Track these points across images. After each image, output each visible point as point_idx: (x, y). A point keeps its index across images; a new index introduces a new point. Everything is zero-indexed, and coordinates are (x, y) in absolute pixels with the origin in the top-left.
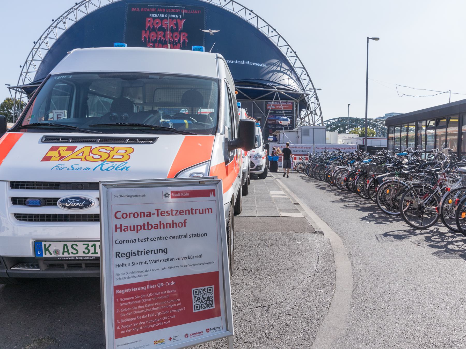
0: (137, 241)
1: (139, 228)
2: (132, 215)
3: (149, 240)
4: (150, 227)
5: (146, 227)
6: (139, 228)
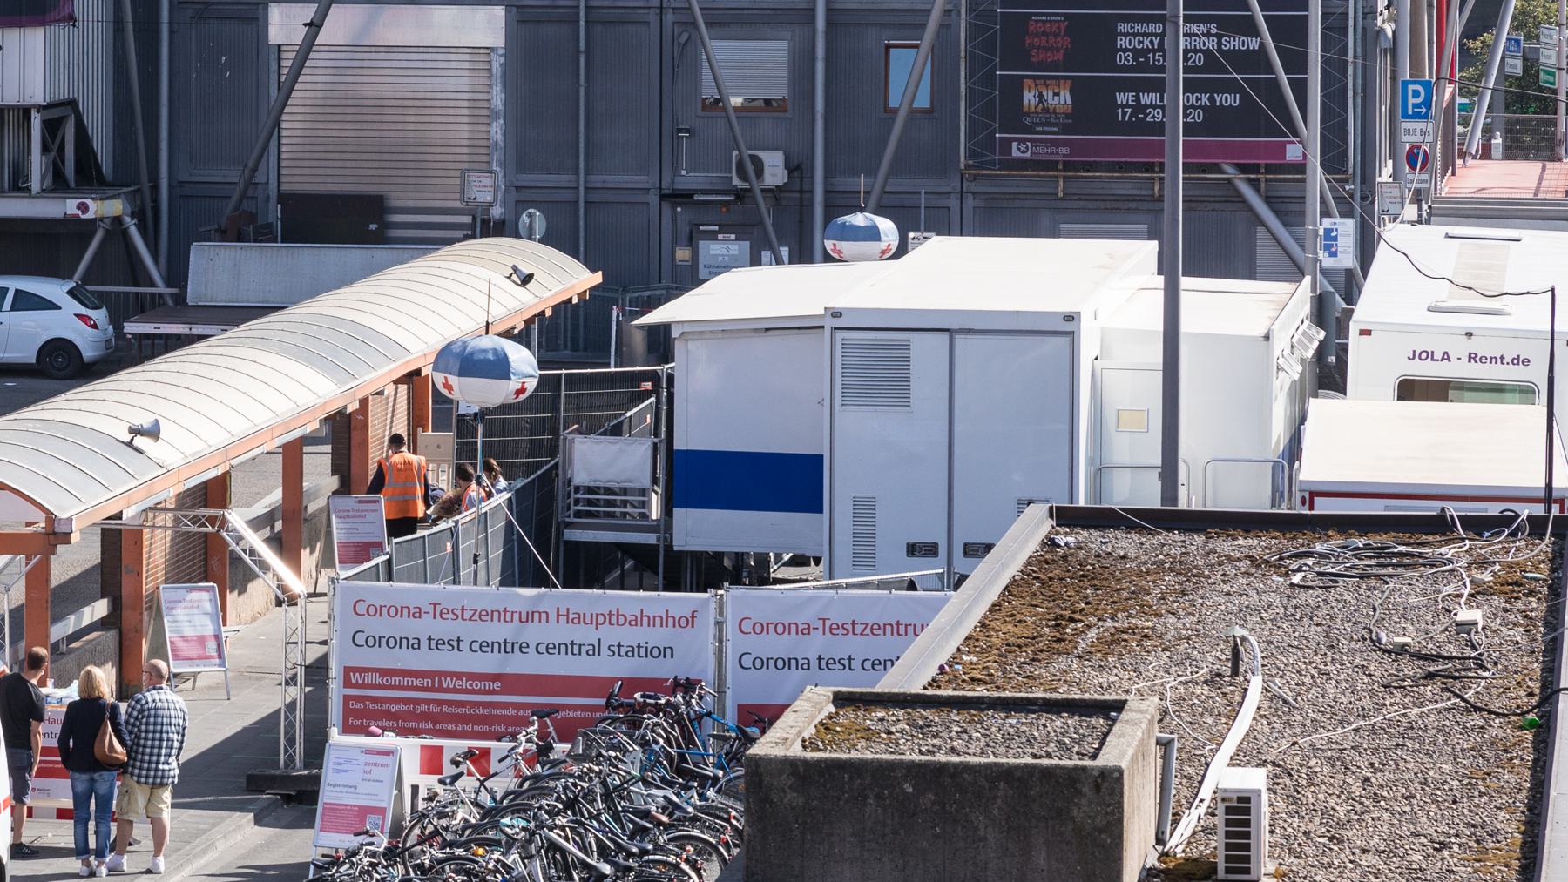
0: (424, 644)
1: (601, 619)
2: (772, 627)
3: (464, 646)
4: (622, 620)
5: (614, 620)
6: (601, 619)
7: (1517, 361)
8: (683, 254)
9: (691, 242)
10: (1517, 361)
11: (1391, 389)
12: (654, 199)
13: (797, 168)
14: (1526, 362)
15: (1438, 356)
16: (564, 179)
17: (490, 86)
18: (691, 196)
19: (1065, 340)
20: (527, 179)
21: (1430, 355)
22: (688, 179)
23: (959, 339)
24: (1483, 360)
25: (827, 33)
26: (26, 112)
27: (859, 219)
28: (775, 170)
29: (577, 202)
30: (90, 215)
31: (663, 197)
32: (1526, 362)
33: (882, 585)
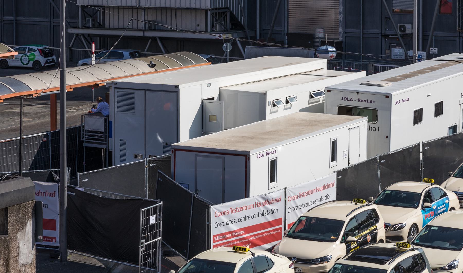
3: (237, 221)
7: (371, 102)
8: (388, 51)
9: (390, 48)
10: (371, 102)
11: (336, 109)
12: (380, 36)
14: (374, 102)
15: (349, 99)
16: (357, 31)
17: (339, 5)
18: (389, 36)
19: (175, 94)
20: (348, 30)
21: (347, 99)
22: (389, 31)
23: (147, 92)
24: (362, 101)
26: (206, 11)
27: (324, 47)
29: (360, 37)
30: (222, 38)
31: (382, 36)
32: (374, 102)
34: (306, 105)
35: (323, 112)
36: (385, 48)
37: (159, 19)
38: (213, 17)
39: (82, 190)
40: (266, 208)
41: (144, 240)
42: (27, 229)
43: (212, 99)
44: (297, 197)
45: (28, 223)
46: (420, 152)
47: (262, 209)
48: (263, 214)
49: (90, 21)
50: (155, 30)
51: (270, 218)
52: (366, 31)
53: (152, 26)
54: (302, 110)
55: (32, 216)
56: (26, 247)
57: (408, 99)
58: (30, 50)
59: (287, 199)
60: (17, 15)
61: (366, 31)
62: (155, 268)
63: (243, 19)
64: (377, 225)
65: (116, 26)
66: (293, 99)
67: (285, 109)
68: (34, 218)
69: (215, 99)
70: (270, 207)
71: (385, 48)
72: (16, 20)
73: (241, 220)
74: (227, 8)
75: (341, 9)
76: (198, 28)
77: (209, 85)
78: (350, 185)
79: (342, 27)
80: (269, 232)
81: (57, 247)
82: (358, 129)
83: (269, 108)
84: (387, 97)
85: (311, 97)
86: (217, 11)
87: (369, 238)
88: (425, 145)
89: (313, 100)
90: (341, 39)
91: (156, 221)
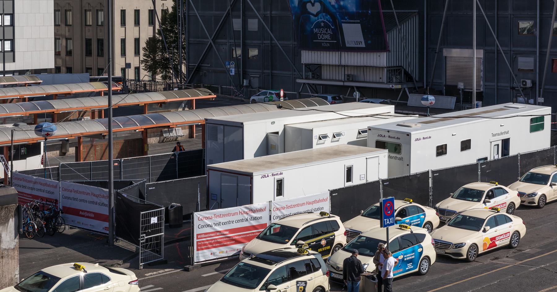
7: (398, 138)
11: (374, 144)
13: (534, 83)
14: (399, 139)
20: (487, 84)
22: (515, 85)
24: (391, 137)
25: (539, 56)
28: (529, 84)
32: (399, 139)
33: (77, 182)
34: (355, 139)
35: (366, 146)
36: (513, 97)
37: (356, 73)
38: (390, 73)
39: (126, 196)
40: (250, 215)
41: (145, 235)
42: (9, 224)
43: (277, 133)
44: (284, 208)
45: (11, 220)
46: (429, 178)
47: (246, 216)
48: (247, 220)
49: (310, 74)
50: (352, 81)
51: (254, 223)
52: (499, 84)
53: (350, 78)
54: (349, 143)
55: (15, 215)
56: (8, 236)
57: (430, 137)
58: (270, 93)
59: (272, 210)
60: (272, 69)
61: (499, 84)
62: (160, 254)
63: (415, 75)
64: (336, 233)
65: (328, 78)
66: (339, 135)
67: (332, 142)
68: (17, 217)
69: (280, 133)
70: (254, 215)
71: (513, 97)
72: (272, 73)
73: (225, 223)
74: (401, 66)
75: (482, 68)
76: (381, 81)
77: (273, 123)
78: (348, 201)
79: (483, 81)
80: (253, 233)
81: (107, 234)
82: (377, 159)
83: (315, 141)
84: (408, 135)
85: (360, 133)
86: (393, 68)
87: (323, 242)
88: (433, 172)
89: (361, 136)
90: (482, 90)
91: (158, 221)
